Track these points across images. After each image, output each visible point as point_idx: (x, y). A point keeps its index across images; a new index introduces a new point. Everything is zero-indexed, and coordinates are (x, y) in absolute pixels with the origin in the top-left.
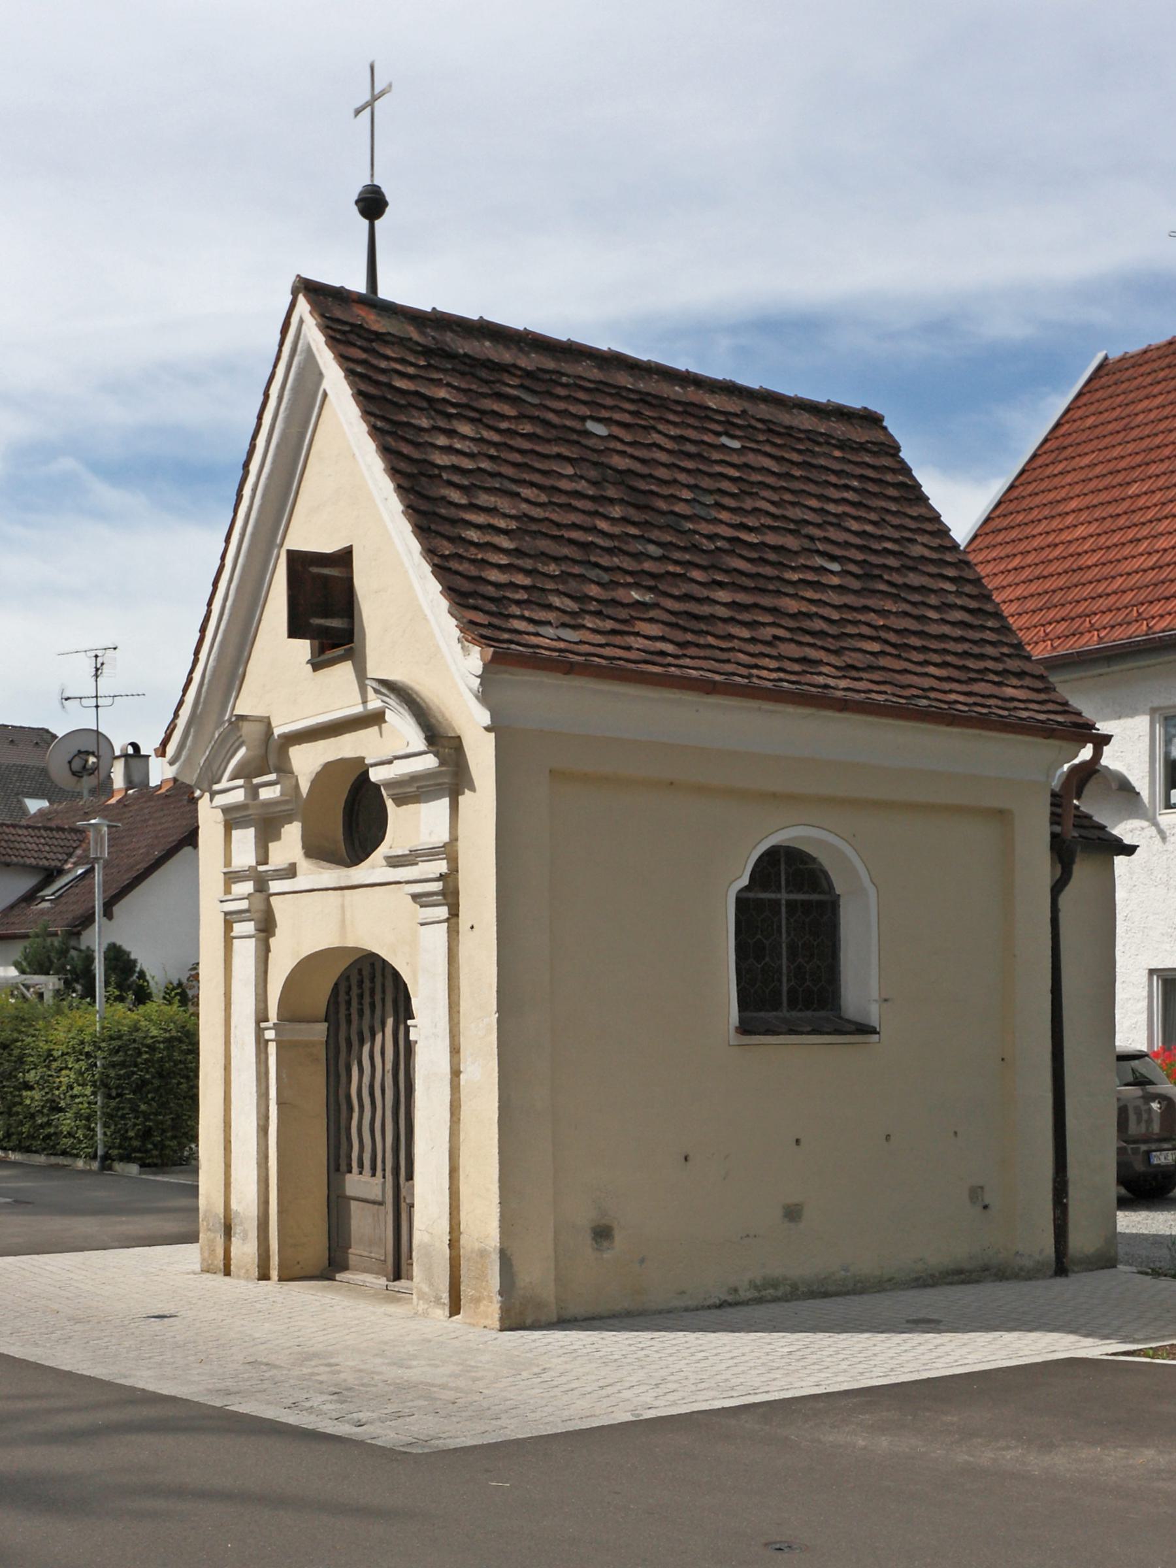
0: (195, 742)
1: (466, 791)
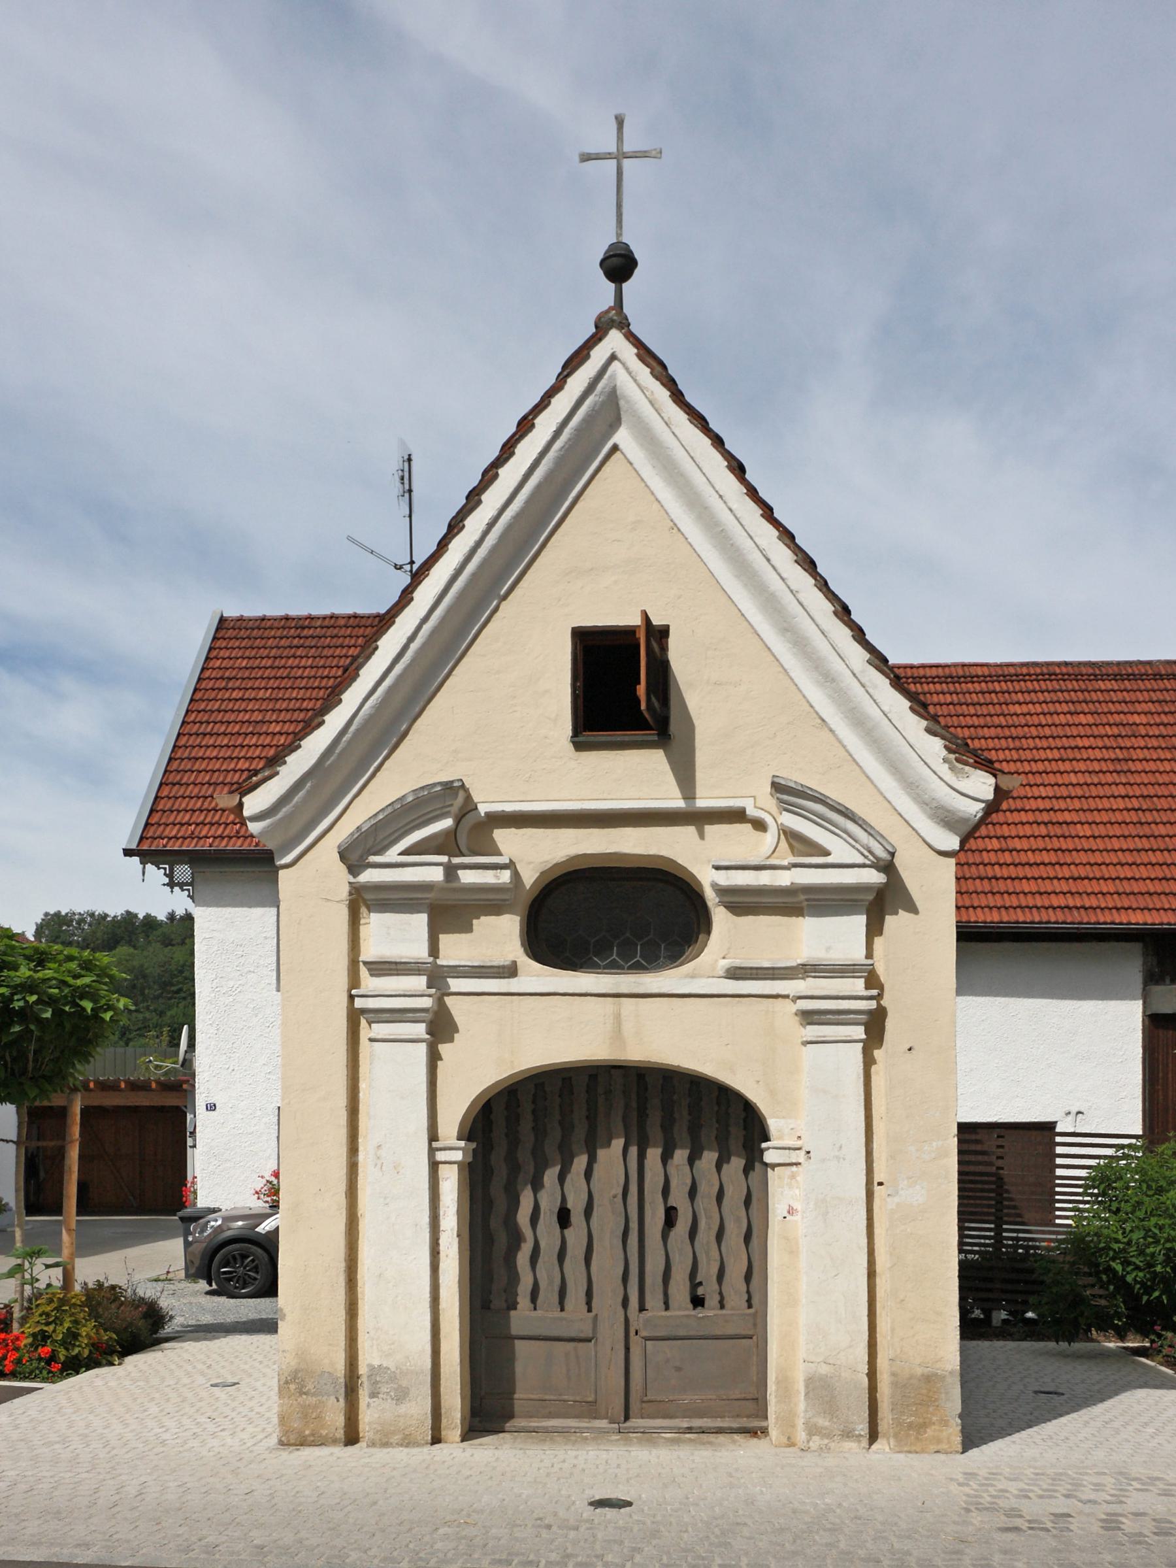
0: (305, 800)
1: (900, 911)
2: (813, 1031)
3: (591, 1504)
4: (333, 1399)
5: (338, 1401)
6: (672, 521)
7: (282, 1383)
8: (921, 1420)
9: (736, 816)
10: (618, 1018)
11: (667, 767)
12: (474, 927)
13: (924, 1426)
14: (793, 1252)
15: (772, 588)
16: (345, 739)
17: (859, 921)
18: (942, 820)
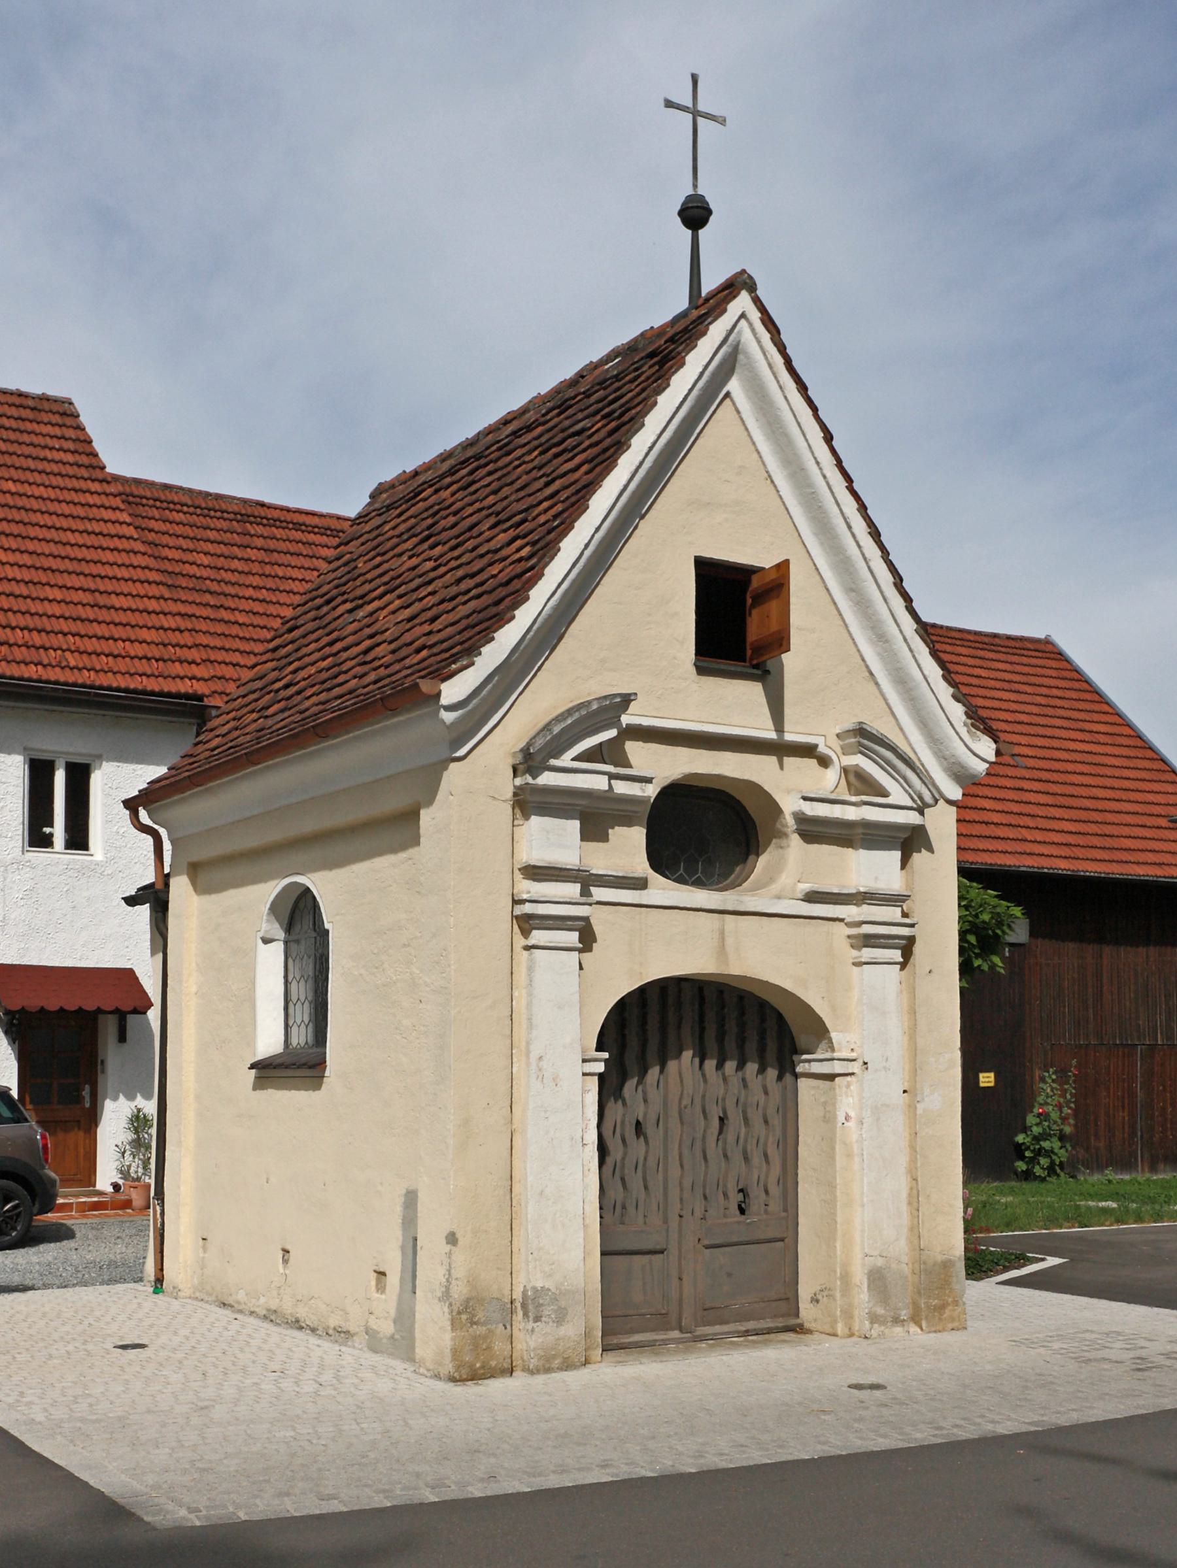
2: (868, 953)
3: (886, 1388)
4: (501, 1326)
5: (506, 1328)
6: (767, 472)
7: (454, 1314)
8: (942, 1302)
9: (807, 751)
10: (722, 933)
11: (763, 700)
12: (610, 837)
13: (942, 1308)
14: (849, 1156)
15: (849, 552)
16: (529, 637)
17: (897, 854)
18: (955, 774)
